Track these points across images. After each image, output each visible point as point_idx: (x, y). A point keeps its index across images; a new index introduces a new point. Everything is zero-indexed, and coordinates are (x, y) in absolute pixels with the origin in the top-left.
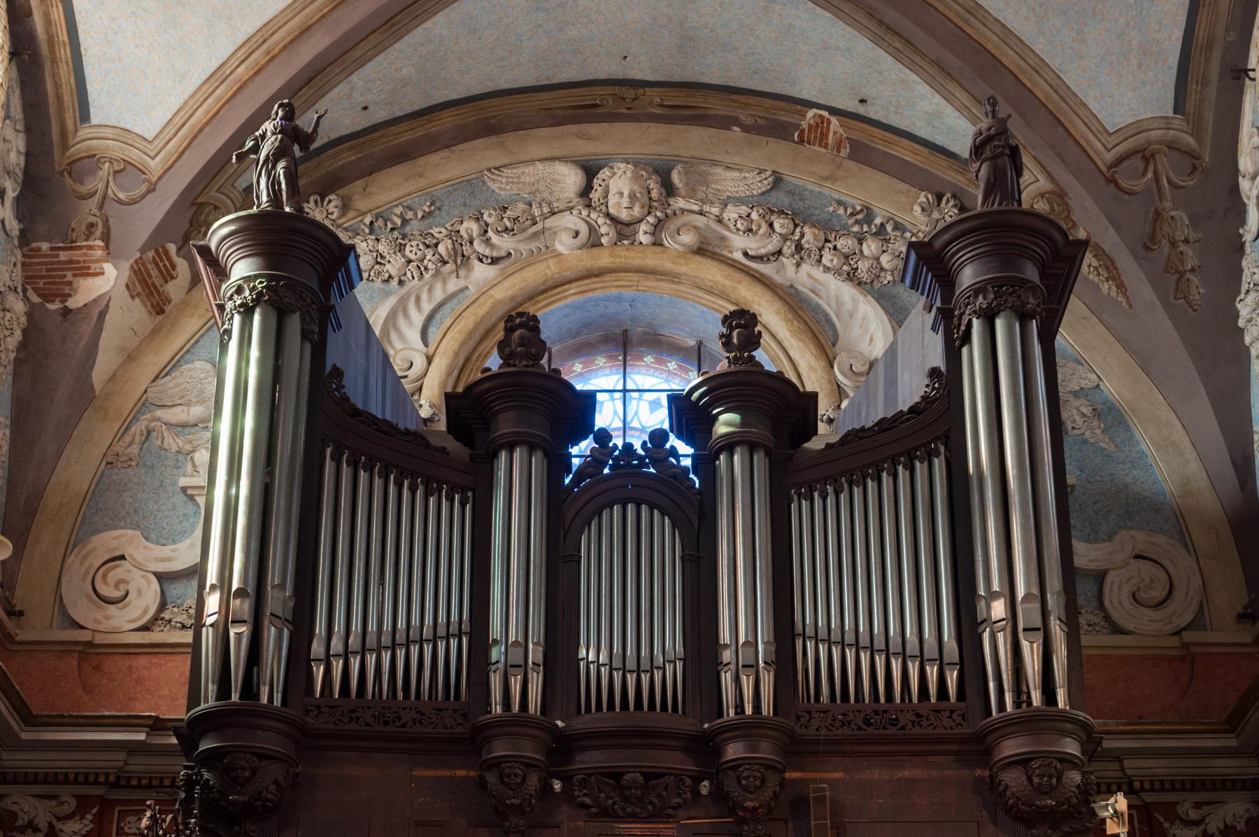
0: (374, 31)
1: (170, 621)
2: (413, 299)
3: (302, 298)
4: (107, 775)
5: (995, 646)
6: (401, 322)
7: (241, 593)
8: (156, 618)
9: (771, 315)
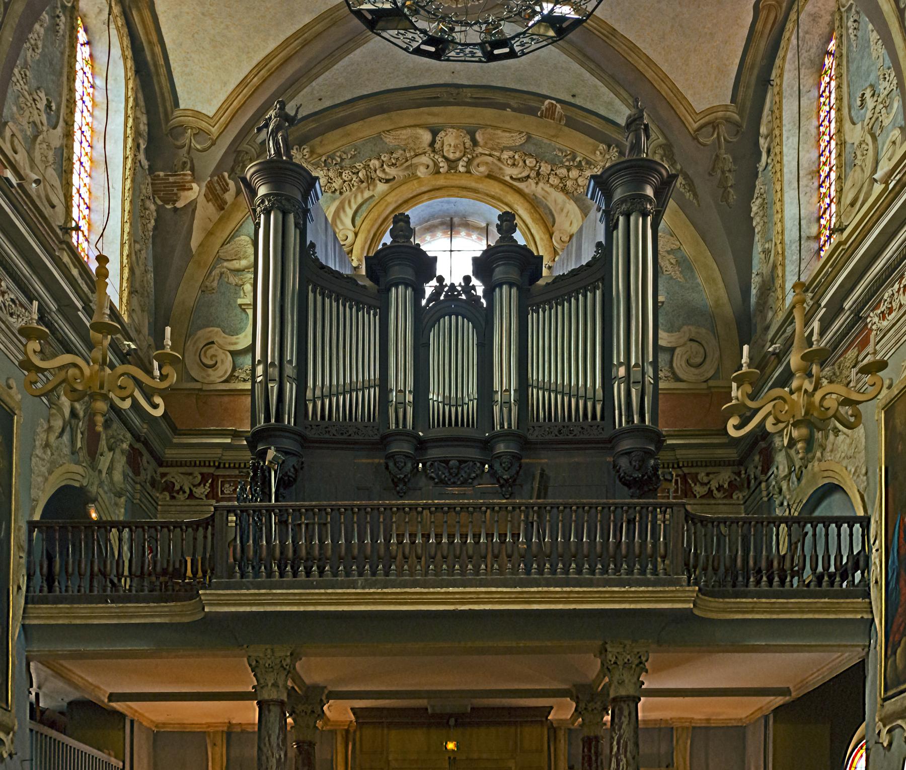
0: (323, 60)
1: (238, 377)
2: (347, 202)
3: (294, 206)
4: (214, 462)
5: (619, 390)
6: (342, 215)
7: (272, 364)
8: (231, 375)
9: (522, 211)
